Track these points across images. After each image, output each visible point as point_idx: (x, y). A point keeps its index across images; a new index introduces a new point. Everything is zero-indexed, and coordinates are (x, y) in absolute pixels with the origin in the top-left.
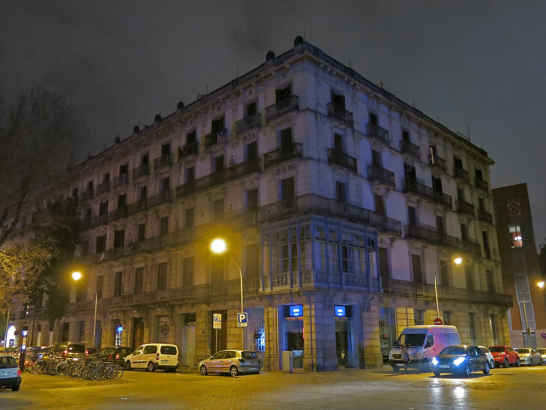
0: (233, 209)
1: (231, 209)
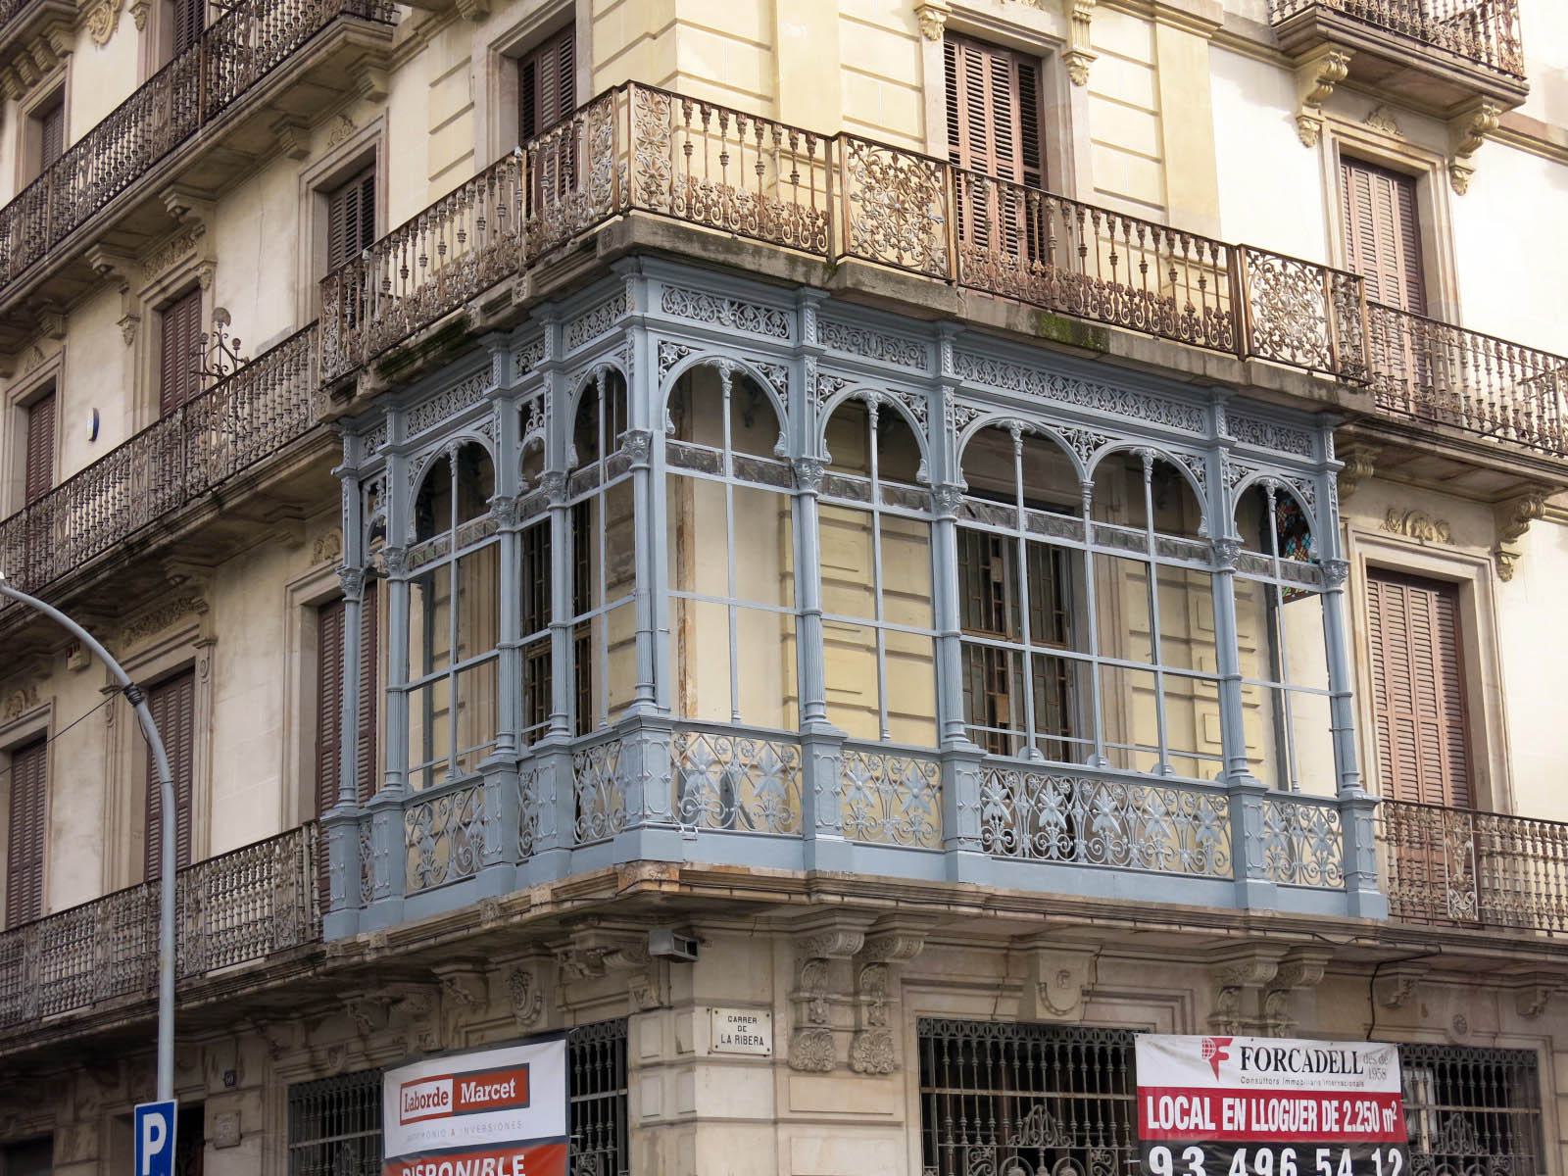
0: (237, 343)
1: (221, 345)
